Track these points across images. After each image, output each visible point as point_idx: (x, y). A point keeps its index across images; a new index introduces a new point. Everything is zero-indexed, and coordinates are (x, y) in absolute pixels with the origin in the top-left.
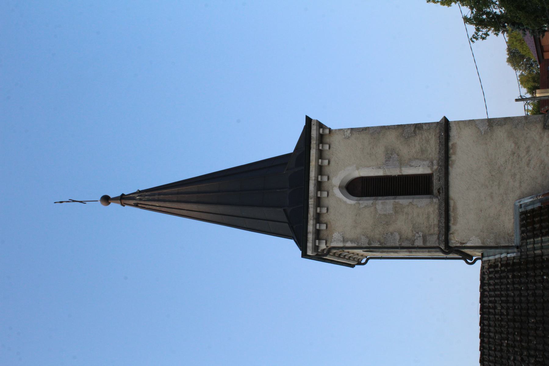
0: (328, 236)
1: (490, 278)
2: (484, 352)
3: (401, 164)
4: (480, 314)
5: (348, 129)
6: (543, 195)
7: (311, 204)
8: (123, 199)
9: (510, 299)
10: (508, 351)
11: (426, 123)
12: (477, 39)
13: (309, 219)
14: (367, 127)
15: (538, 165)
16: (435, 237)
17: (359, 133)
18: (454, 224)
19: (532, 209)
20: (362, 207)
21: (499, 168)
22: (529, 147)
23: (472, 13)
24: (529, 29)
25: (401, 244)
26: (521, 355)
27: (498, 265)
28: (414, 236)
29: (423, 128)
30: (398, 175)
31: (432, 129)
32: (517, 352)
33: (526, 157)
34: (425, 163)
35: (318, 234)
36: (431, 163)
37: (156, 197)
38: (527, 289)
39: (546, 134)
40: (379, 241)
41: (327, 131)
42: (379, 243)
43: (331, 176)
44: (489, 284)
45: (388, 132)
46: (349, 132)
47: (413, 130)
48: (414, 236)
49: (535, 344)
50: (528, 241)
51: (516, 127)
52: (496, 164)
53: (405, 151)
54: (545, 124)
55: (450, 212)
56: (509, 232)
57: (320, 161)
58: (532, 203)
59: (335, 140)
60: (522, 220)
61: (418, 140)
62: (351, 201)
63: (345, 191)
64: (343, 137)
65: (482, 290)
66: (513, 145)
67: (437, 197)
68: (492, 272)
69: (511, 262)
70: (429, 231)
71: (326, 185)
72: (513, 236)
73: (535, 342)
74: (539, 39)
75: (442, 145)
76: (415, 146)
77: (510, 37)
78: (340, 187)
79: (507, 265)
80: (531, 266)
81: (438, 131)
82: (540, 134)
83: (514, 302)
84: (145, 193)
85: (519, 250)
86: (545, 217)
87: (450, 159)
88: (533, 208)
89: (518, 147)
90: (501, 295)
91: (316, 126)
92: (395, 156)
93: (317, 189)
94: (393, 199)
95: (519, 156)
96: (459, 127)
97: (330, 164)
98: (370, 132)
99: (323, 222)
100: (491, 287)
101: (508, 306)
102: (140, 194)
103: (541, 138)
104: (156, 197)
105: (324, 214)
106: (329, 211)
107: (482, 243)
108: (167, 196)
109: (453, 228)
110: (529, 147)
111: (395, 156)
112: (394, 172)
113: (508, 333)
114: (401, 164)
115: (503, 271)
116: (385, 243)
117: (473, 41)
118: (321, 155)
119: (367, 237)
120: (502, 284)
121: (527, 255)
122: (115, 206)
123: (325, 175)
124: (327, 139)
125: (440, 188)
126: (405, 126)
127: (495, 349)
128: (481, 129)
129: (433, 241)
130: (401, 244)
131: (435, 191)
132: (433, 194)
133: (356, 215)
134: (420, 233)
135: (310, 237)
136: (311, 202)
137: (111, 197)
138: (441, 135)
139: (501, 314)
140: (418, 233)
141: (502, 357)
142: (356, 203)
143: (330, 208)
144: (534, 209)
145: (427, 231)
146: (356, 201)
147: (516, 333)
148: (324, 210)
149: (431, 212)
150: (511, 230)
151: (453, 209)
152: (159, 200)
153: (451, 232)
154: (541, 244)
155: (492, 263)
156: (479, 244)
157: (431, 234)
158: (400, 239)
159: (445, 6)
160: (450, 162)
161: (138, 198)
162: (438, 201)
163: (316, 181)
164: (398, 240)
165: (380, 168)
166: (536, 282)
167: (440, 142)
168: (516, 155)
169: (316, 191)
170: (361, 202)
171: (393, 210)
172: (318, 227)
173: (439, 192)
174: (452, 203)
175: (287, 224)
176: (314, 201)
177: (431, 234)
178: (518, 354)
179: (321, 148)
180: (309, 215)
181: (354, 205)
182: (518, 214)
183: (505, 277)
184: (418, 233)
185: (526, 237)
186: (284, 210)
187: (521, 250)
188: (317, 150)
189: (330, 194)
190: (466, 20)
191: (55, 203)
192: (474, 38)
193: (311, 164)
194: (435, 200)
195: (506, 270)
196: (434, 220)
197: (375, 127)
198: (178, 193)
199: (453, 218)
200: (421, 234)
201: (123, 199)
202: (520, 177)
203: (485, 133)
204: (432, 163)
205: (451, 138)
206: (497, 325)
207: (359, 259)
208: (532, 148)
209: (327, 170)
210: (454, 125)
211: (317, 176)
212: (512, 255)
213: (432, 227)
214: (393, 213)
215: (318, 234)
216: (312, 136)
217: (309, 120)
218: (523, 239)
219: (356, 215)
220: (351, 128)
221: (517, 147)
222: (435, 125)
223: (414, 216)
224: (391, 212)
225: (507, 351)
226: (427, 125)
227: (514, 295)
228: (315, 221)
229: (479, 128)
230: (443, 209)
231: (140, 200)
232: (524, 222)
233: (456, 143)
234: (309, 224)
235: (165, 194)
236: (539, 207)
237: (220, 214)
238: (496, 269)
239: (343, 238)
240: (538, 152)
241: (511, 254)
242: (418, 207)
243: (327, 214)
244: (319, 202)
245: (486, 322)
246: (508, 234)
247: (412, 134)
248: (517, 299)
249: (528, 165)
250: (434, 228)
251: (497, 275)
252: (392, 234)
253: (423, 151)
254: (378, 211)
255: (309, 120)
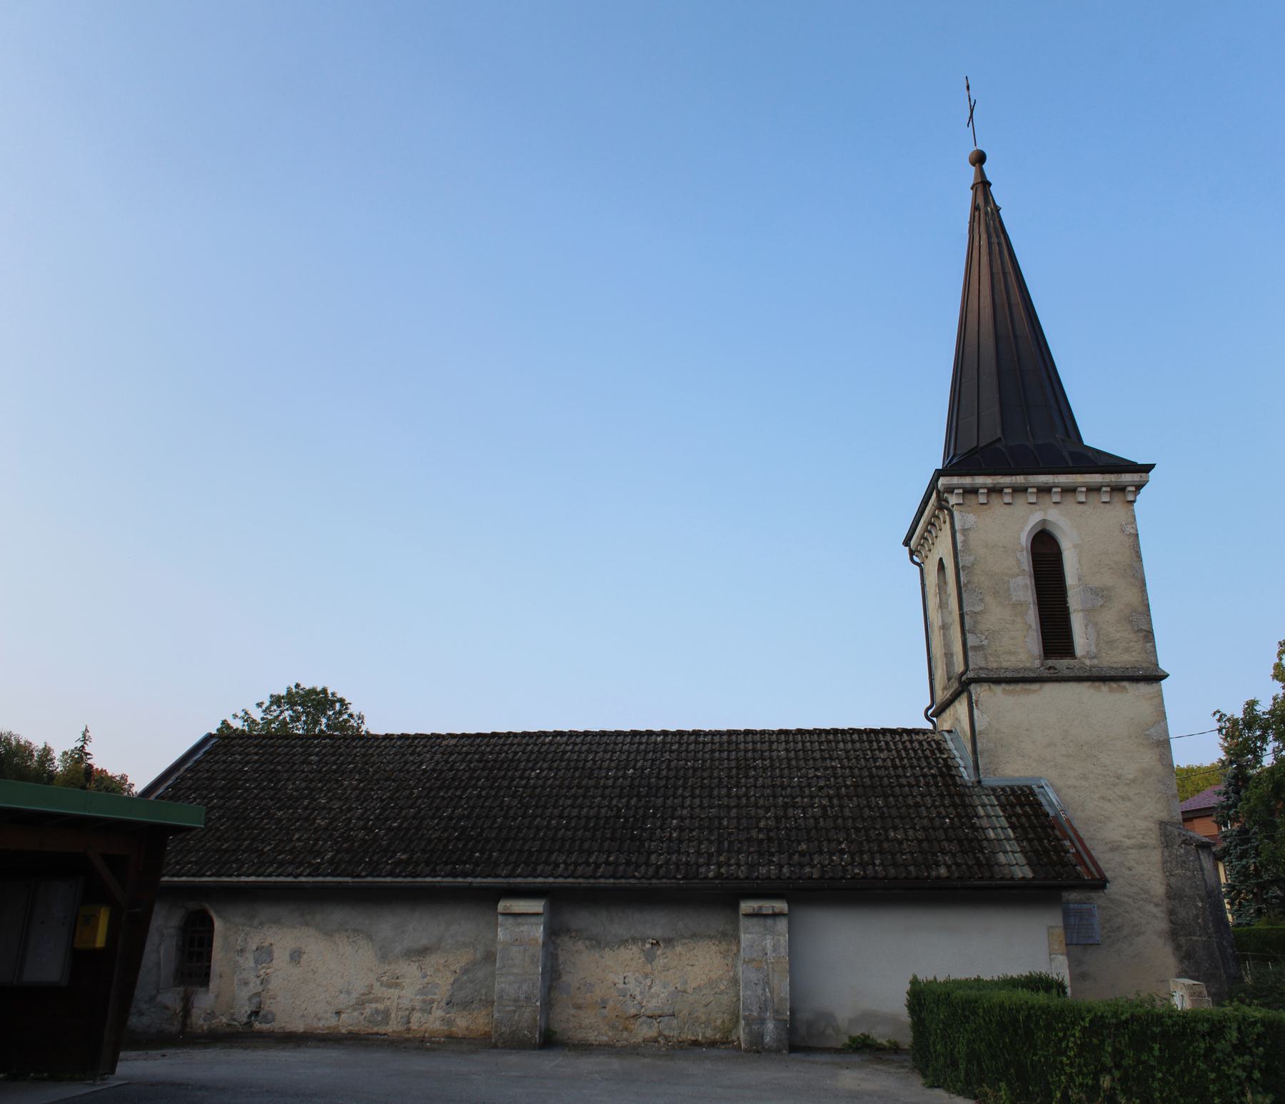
0: (969, 506)
1: (920, 743)
2: (813, 735)
3: (1088, 612)
4: (866, 729)
5: (1137, 530)
6: (1067, 820)
7: (1016, 479)
8: (982, 186)
9: (900, 771)
10: (826, 768)
11: (1155, 647)
12: (1219, 720)
13: (993, 477)
14: (1141, 558)
15: (1104, 813)
16: (983, 664)
17: (1132, 547)
18: (1004, 690)
19: (1041, 803)
20: (1018, 555)
21: (1095, 756)
22: (1130, 800)
23: (1264, 713)
24: (1228, 800)
25: (967, 614)
26: (828, 787)
27: (944, 754)
28: (982, 633)
29: (1147, 642)
30: (1068, 607)
31: (1147, 657)
32: (829, 780)
33: (1114, 796)
34: (1093, 646)
35: (972, 491)
36: (1093, 655)
37: (994, 240)
38: (923, 796)
39: (1152, 825)
40: (968, 582)
41: (1130, 498)
42: (965, 582)
43: (1060, 506)
44: (911, 742)
45: (1136, 591)
46: (1133, 531)
47: (1143, 628)
48: (982, 633)
49: (848, 806)
50: (992, 797)
51: (1159, 781)
52: (1100, 752)
53: (1108, 617)
54: (1168, 824)
55: (1021, 684)
56: (999, 770)
57: (1084, 489)
58: (1051, 804)
59: (1116, 511)
60: (1020, 788)
61: (1128, 636)
62: (1024, 539)
63: (1039, 529)
64: (1124, 523)
65: (900, 731)
66: (1131, 777)
67: (1042, 666)
68: (931, 746)
69: (954, 772)
70: (990, 654)
71: (1046, 499)
72: (995, 775)
73: (851, 805)
74: (1211, 815)
75: (1124, 672)
76: (1118, 631)
77: (1211, 770)
78: (1044, 521)
79: (949, 767)
80: (958, 801)
81: (1144, 665)
82: (1151, 817)
83: (898, 777)
84: (997, 219)
85: (976, 784)
86: (1035, 822)
87: (1101, 684)
88: (1044, 804)
89: (1128, 784)
90: (901, 759)
91: (1138, 480)
92: (1100, 602)
93: (1040, 487)
94: (1034, 601)
95: (1115, 785)
96: (1152, 698)
97: (1078, 505)
98: (1134, 563)
99: (989, 499)
100: (908, 744)
101: (889, 768)
102: (994, 211)
103: (1146, 818)
104: (994, 240)
105: (1002, 499)
106: (1007, 507)
107: (980, 731)
108: (998, 257)
109: (998, 689)
110: (1130, 800)
111: (1100, 602)
112: (1075, 600)
113: (851, 768)
114: (1088, 611)
115: (936, 760)
116: (968, 591)
117: (1214, 714)
118: (1094, 489)
119: (973, 564)
120: (919, 759)
121: (971, 796)
122: (969, 174)
123: (1061, 497)
124: (1118, 497)
125: (1056, 669)
126: (1149, 615)
127: (823, 751)
128: (1152, 730)
129: (976, 660)
130: (967, 614)
131: (1050, 662)
132: (1045, 659)
133: (1004, 547)
134: (986, 641)
135: (967, 481)
136: (1020, 479)
137: (984, 166)
138: (1139, 670)
139: (875, 760)
140: (986, 638)
141: (815, 759)
142: (1023, 547)
143: (1012, 507)
144: (1043, 806)
145: (990, 651)
146: (1025, 546)
147: (854, 780)
148: (1007, 499)
149: (1019, 657)
150: (1002, 773)
151: (1026, 690)
152: (990, 244)
153: (992, 686)
154: (994, 816)
155: (944, 745)
156: (977, 728)
157: (986, 658)
158: (975, 613)
159: (1273, 671)
160: (1097, 684)
161: (989, 209)
162: (1036, 666)
163: (1051, 485)
164: (972, 609)
165: (1080, 580)
166: (936, 807)
167: (1127, 668)
168: (1116, 780)
169: (1036, 485)
170: (1025, 552)
171: (1016, 601)
172: (981, 491)
173: (1050, 668)
174: (1035, 686)
175: (975, 444)
176: (1021, 483)
177: (986, 658)
178: (827, 783)
179: (1104, 489)
180: (999, 477)
181: (1020, 543)
182: (1028, 783)
183: (929, 763)
184: (986, 638)
185: (997, 794)
186: (999, 439)
187: (976, 787)
188: (1100, 485)
189: (1032, 506)
190: (1251, 705)
191: (967, 77)
192: (1221, 716)
193: (1078, 475)
194: (1037, 663)
195: (940, 765)
196: (1008, 661)
197: (1143, 571)
198: (1004, 273)
199: (1013, 690)
200: (985, 643)
201: (982, 186)
202: (1082, 787)
203: (1145, 735)
204: (1094, 658)
205: (1134, 684)
206: (858, 753)
207: (919, 552)
208: (1128, 804)
209: (1069, 498)
210: (1155, 690)
211: (1060, 485)
212: (965, 775)
213: (997, 659)
214: (1012, 602)
215: (972, 491)
216: (1123, 475)
217: (1147, 468)
218: (994, 790)
219: (1004, 547)
220: (1138, 534)
221: (1128, 782)
222: (1153, 661)
223: (1011, 633)
224: (1014, 599)
225: (826, 767)
226: (1152, 649)
227: (907, 777)
228: (991, 486)
229: (1153, 726)
230: (1027, 674)
231: (986, 213)
232: (1019, 792)
233: (1127, 692)
234: (986, 477)
235: (1001, 253)
236: (1048, 813)
237: (979, 342)
238: (936, 751)
239: (969, 529)
240: (1123, 813)
241: (966, 773)
242: (1025, 637)
243: (1002, 503)
244: (1020, 490)
245: (855, 737)
246: (996, 769)
247: (1136, 627)
248: (903, 781)
249: (1103, 798)
250: (996, 661)
251: (928, 753)
252: (982, 600)
253: (1111, 643)
254: (1014, 579)
255: (1147, 468)
